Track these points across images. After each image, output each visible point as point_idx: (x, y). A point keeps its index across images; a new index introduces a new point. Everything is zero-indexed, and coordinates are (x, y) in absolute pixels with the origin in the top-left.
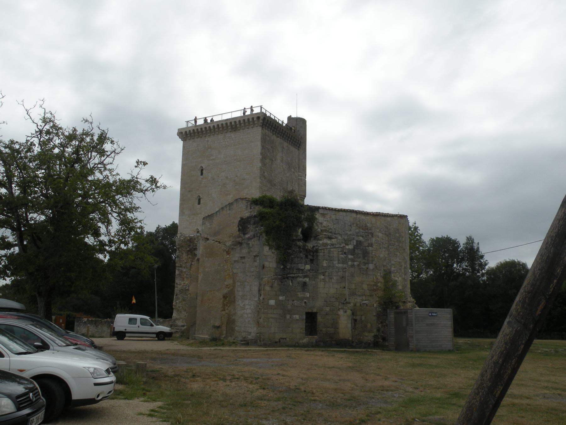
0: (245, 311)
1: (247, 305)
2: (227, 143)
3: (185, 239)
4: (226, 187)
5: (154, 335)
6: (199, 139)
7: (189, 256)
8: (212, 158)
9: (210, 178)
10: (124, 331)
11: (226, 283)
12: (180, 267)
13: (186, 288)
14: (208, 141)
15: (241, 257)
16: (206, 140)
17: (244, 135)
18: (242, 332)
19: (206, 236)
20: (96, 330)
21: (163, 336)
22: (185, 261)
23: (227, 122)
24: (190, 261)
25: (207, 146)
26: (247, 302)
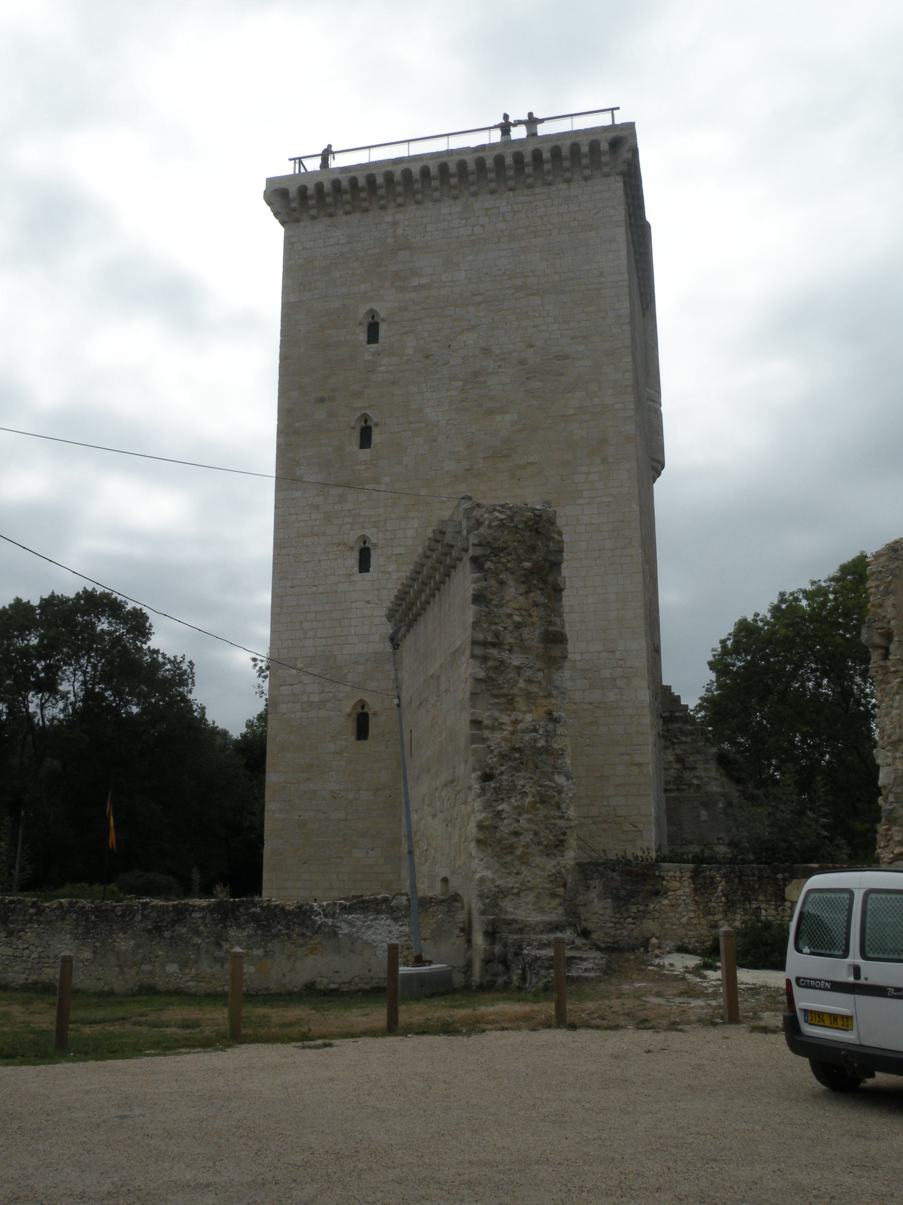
2: (477, 229)
3: (511, 518)
4: (485, 382)
6: (357, 216)
7: (532, 595)
8: (415, 282)
9: (410, 351)
12: (494, 645)
13: (536, 741)
14: (395, 224)
16: (388, 218)
17: (553, 205)
20: (9, 951)
22: (517, 618)
23: (481, 154)
24: (535, 619)
25: (390, 240)
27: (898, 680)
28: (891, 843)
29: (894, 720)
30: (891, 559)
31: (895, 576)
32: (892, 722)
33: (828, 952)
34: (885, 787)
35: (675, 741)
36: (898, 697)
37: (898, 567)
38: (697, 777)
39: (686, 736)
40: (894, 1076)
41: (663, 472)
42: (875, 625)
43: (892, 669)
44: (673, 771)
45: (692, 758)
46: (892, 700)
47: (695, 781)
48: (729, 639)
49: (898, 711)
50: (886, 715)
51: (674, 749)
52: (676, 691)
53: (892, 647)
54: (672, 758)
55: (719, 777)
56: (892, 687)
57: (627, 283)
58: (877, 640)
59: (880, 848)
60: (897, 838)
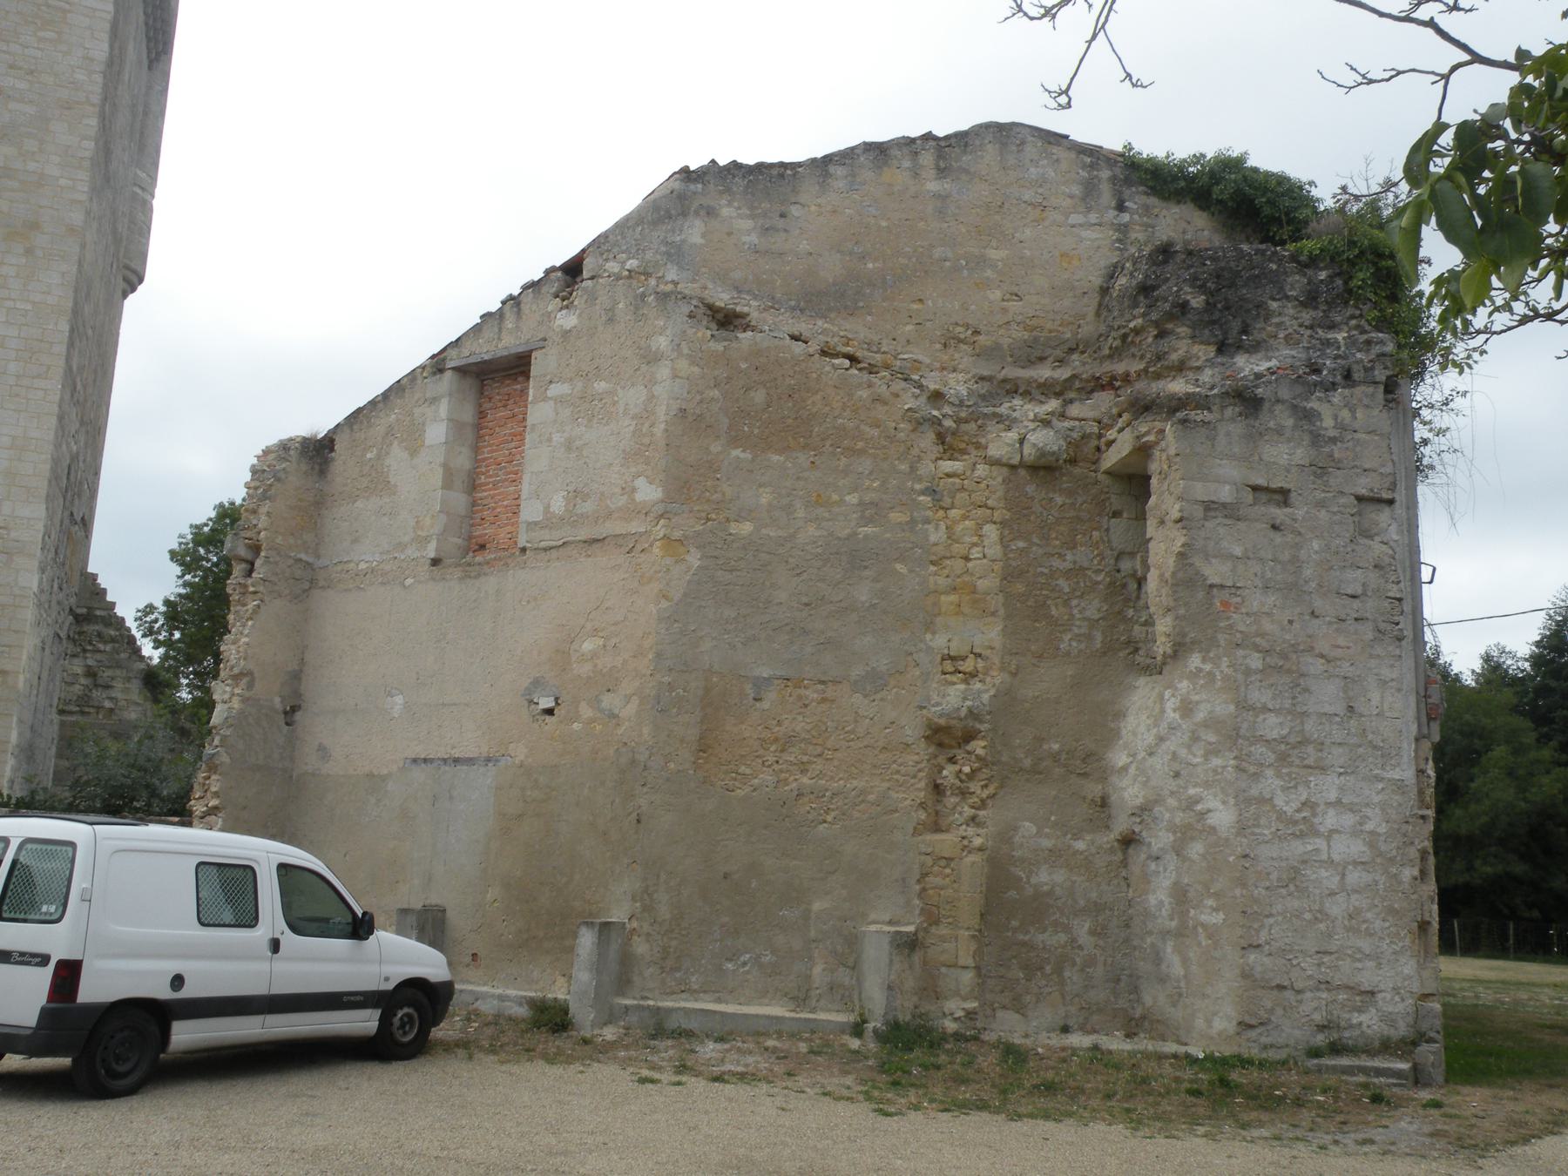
0: (1320, 843)
1: (1329, 804)
5: (366, 1013)
10: (164, 993)
11: (939, 641)
15: (1255, 488)
18: (1299, 992)
19: (722, 298)
21: (406, 1010)
26: (1328, 787)
27: (255, 603)
28: (209, 794)
29: (241, 649)
30: (281, 459)
31: (278, 480)
32: (238, 652)
33: (22, 916)
34: (215, 727)
35: (89, 648)
36: (250, 623)
37: (284, 469)
38: (111, 699)
39: (105, 643)
40: (62, 1059)
41: (140, 288)
42: (243, 534)
43: (251, 589)
44: (78, 687)
45: (109, 673)
46: (244, 626)
47: (108, 704)
48: (206, 525)
49: (246, 640)
50: (234, 643)
51: (86, 658)
52: (103, 581)
53: (258, 563)
54: (79, 670)
55: (141, 702)
56: (247, 610)
57: (109, 17)
58: (242, 552)
59: (195, 799)
60: (214, 789)
